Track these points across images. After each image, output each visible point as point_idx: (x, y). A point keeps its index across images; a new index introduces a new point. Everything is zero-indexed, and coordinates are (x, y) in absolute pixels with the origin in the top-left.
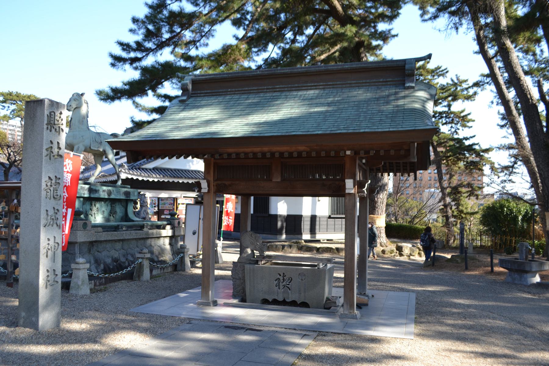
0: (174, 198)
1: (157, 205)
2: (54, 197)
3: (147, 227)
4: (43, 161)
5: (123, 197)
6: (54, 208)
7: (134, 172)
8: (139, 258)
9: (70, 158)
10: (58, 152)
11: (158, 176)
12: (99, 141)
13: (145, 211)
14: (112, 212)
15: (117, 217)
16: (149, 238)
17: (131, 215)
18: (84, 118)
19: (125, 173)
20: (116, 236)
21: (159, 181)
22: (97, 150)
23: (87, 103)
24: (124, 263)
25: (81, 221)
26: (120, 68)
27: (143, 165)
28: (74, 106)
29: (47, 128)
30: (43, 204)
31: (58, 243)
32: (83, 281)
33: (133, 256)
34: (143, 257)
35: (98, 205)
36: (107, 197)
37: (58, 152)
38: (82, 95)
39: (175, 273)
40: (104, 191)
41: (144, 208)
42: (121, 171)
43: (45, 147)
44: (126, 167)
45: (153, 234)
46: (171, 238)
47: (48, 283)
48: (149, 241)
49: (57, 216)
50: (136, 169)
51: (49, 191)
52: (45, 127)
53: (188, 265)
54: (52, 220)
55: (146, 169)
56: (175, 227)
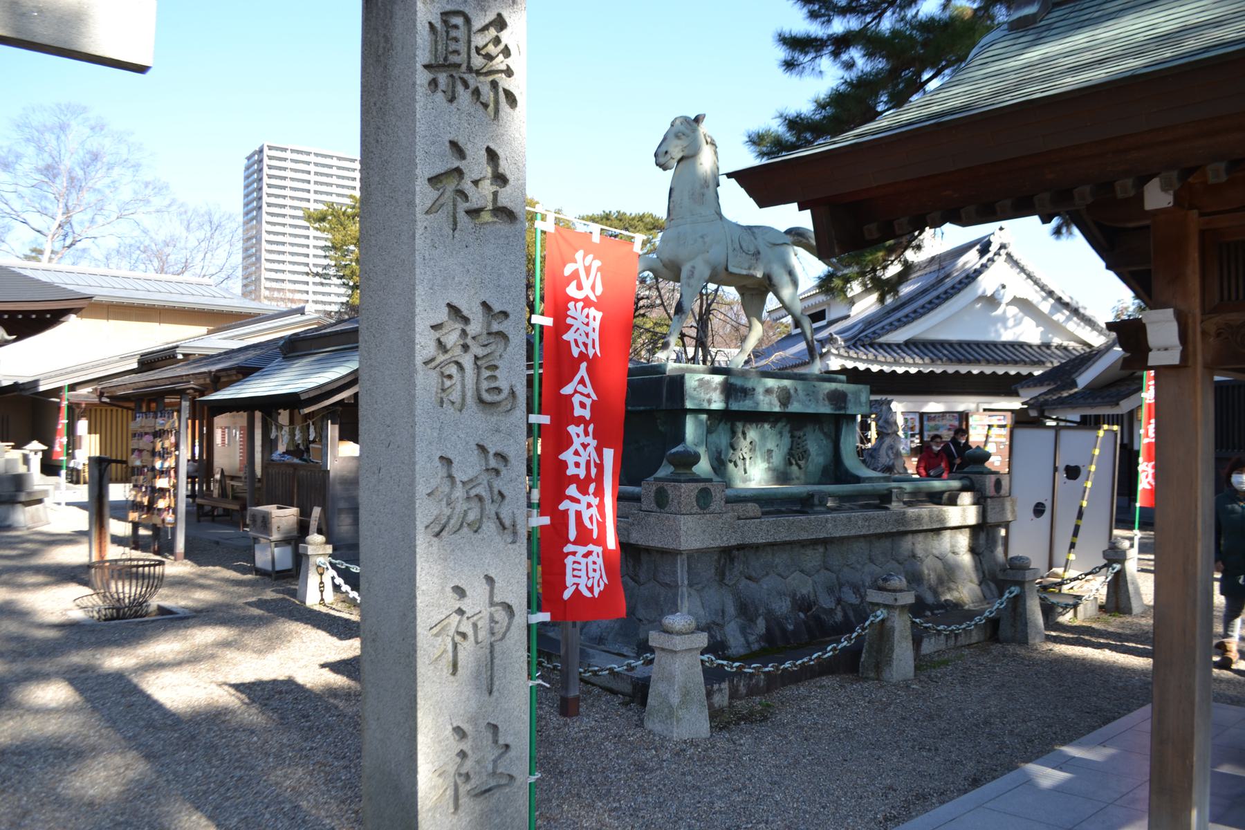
0: (961, 414)
1: (917, 430)
2: (481, 401)
3: (899, 500)
4: (419, 231)
5: (826, 409)
6: (482, 448)
7: (861, 354)
8: (878, 605)
9: (590, 249)
10: (495, 194)
11: (918, 360)
12: (752, 250)
13: (891, 447)
14: (795, 454)
15: (811, 468)
16: (906, 533)
17: (851, 462)
18: (705, 184)
19: (839, 356)
20: (804, 529)
21: (919, 372)
22: (747, 276)
23: (713, 144)
24: (831, 612)
25: (692, 485)
26: (808, 71)
27: (880, 336)
28: (677, 154)
29: (434, 83)
30: (424, 429)
31: (508, 608)
32: (686, 694)
33: (857, 589)
34: (891, 602)
35: (752, 434)
36: (777, 409)
37: (495, 194)
38: (698, 120)
39: (996, 649)
40: (768, 391)
41: (888, 441)
42: (829, 351)
43: (424, 171)
44: (841, 342)
45: (918, 519)
46: (975, 530)
47: (463, 789)
48: (907, 544)
49: (498, 484)
50: (863, 346)
51: (453, 370)
52: (423, 77)
53: (1036, 626)
54: (475, 504)
55: (889, 345)
56: (985, 498)
